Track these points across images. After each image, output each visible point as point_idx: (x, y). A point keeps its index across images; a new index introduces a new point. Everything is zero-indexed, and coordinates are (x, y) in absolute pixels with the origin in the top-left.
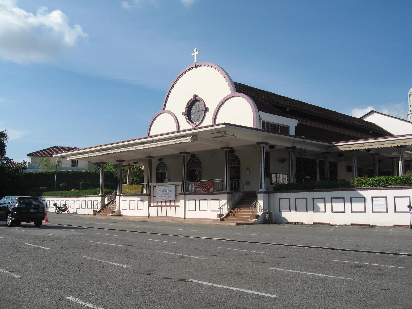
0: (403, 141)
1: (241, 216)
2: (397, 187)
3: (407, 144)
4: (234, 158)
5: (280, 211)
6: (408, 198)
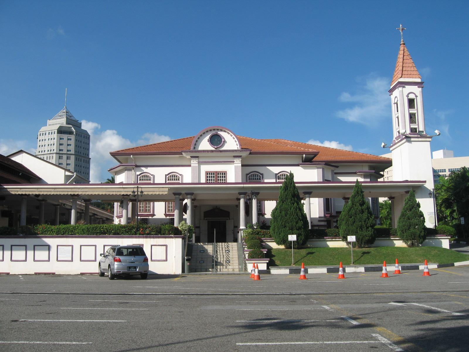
0: (80, 190)
2: (84, 236)
4: (148, 209)
6: (94, 246)
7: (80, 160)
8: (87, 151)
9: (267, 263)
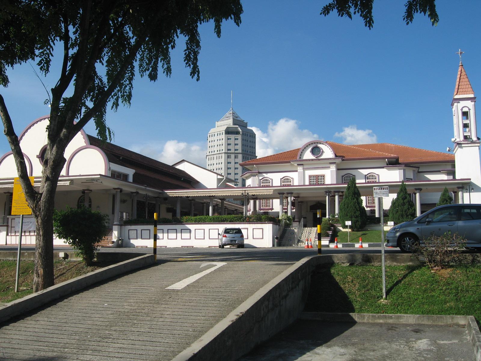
0: (214, 192)
1: (238, 206)
3: (216, 195)
5: (129, 239)
7: (245, 157)
8: (253, 149)
9: (329, 240)
